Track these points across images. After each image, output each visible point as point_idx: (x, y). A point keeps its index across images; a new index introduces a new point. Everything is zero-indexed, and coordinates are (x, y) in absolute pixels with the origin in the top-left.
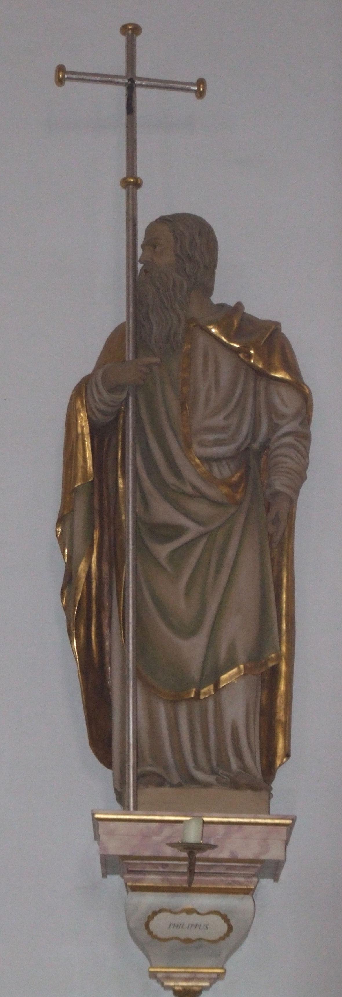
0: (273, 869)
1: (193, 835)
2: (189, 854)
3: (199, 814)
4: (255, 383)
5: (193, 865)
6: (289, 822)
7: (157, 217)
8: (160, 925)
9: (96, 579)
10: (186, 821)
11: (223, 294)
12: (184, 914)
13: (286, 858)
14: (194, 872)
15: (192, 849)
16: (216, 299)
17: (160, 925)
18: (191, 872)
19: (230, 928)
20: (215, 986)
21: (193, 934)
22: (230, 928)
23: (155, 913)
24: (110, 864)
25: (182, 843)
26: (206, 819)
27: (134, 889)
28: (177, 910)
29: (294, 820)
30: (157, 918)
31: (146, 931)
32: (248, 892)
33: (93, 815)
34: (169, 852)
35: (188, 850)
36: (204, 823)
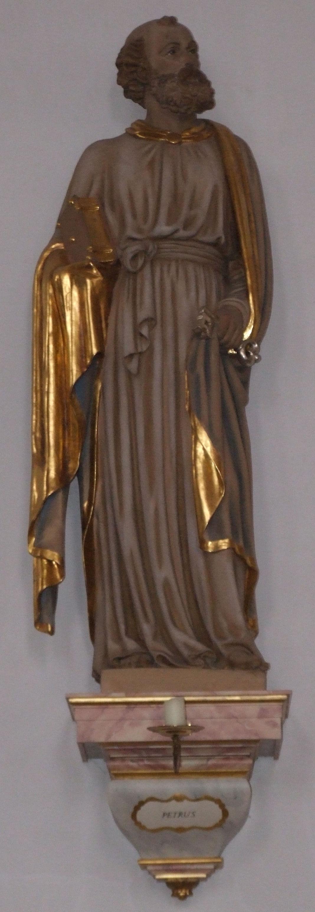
0: (273, 749)
1: (175, 717)
2: (173, 738)
3: (179, 693)
4: (88, 194)
5: (173, 748)
6: (284, 697)
7: (196, 38)
8: (149, 815)
9: (214, 460)
10: (167, 701)
11: (146, 110)
12: (174, 802)
13: (282, 736)
14: (180, 757)
15: (175, 733)
16: (141, 114)
17: (149, 815)
18: (176, 758)
19: (225, 813)
20: (214, 876)
21: (185, 822)
22: (225, 813)
23: (142, 803)
24: (88, 750)
25: (166, 726)
26: (187, 699)
27: (116, 775)
28: (166, 798)
29: (289, 696)
30: (143, 808)
31: (133, 822)
32: (247, 774)
33: (67, 699)
34: (157, 737)
35: (172, 734)
36: (186, 702)
